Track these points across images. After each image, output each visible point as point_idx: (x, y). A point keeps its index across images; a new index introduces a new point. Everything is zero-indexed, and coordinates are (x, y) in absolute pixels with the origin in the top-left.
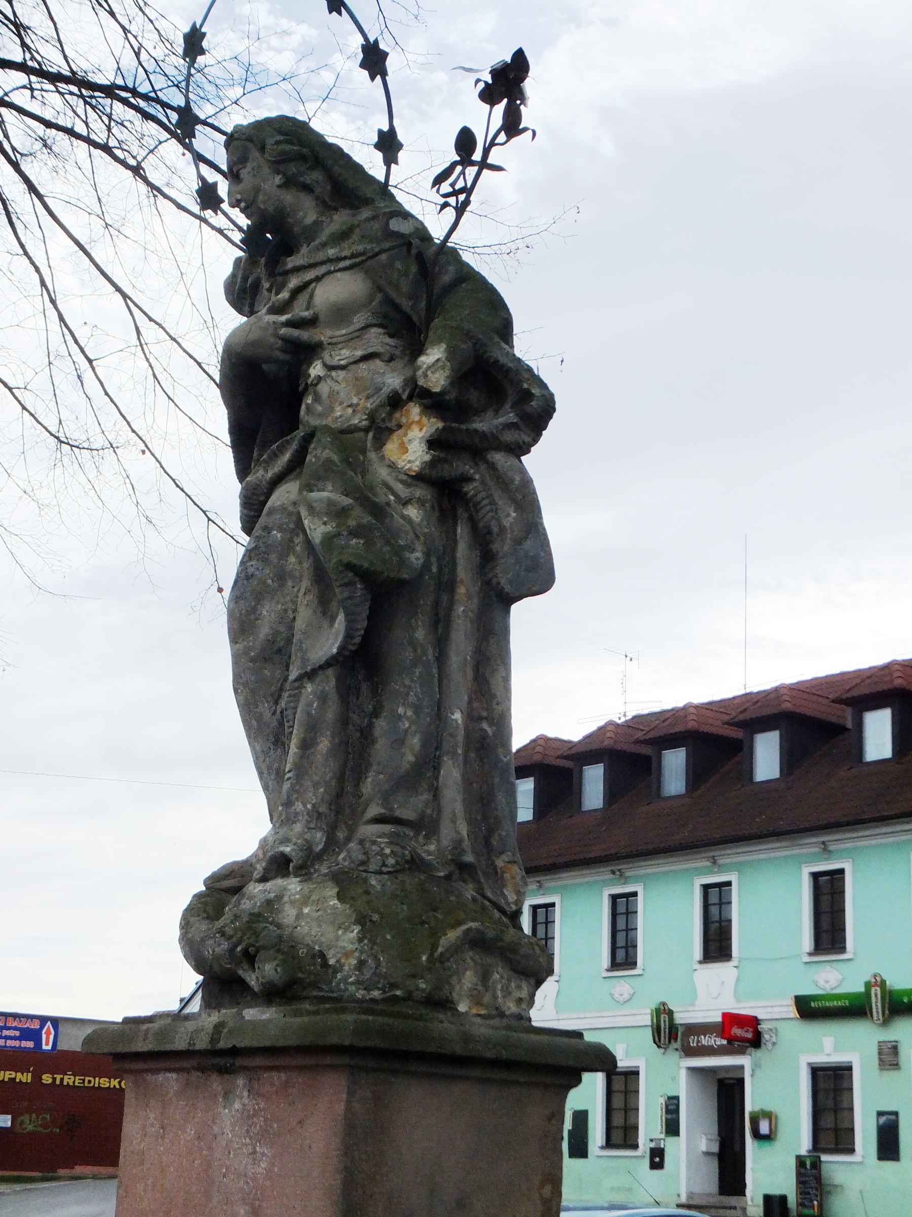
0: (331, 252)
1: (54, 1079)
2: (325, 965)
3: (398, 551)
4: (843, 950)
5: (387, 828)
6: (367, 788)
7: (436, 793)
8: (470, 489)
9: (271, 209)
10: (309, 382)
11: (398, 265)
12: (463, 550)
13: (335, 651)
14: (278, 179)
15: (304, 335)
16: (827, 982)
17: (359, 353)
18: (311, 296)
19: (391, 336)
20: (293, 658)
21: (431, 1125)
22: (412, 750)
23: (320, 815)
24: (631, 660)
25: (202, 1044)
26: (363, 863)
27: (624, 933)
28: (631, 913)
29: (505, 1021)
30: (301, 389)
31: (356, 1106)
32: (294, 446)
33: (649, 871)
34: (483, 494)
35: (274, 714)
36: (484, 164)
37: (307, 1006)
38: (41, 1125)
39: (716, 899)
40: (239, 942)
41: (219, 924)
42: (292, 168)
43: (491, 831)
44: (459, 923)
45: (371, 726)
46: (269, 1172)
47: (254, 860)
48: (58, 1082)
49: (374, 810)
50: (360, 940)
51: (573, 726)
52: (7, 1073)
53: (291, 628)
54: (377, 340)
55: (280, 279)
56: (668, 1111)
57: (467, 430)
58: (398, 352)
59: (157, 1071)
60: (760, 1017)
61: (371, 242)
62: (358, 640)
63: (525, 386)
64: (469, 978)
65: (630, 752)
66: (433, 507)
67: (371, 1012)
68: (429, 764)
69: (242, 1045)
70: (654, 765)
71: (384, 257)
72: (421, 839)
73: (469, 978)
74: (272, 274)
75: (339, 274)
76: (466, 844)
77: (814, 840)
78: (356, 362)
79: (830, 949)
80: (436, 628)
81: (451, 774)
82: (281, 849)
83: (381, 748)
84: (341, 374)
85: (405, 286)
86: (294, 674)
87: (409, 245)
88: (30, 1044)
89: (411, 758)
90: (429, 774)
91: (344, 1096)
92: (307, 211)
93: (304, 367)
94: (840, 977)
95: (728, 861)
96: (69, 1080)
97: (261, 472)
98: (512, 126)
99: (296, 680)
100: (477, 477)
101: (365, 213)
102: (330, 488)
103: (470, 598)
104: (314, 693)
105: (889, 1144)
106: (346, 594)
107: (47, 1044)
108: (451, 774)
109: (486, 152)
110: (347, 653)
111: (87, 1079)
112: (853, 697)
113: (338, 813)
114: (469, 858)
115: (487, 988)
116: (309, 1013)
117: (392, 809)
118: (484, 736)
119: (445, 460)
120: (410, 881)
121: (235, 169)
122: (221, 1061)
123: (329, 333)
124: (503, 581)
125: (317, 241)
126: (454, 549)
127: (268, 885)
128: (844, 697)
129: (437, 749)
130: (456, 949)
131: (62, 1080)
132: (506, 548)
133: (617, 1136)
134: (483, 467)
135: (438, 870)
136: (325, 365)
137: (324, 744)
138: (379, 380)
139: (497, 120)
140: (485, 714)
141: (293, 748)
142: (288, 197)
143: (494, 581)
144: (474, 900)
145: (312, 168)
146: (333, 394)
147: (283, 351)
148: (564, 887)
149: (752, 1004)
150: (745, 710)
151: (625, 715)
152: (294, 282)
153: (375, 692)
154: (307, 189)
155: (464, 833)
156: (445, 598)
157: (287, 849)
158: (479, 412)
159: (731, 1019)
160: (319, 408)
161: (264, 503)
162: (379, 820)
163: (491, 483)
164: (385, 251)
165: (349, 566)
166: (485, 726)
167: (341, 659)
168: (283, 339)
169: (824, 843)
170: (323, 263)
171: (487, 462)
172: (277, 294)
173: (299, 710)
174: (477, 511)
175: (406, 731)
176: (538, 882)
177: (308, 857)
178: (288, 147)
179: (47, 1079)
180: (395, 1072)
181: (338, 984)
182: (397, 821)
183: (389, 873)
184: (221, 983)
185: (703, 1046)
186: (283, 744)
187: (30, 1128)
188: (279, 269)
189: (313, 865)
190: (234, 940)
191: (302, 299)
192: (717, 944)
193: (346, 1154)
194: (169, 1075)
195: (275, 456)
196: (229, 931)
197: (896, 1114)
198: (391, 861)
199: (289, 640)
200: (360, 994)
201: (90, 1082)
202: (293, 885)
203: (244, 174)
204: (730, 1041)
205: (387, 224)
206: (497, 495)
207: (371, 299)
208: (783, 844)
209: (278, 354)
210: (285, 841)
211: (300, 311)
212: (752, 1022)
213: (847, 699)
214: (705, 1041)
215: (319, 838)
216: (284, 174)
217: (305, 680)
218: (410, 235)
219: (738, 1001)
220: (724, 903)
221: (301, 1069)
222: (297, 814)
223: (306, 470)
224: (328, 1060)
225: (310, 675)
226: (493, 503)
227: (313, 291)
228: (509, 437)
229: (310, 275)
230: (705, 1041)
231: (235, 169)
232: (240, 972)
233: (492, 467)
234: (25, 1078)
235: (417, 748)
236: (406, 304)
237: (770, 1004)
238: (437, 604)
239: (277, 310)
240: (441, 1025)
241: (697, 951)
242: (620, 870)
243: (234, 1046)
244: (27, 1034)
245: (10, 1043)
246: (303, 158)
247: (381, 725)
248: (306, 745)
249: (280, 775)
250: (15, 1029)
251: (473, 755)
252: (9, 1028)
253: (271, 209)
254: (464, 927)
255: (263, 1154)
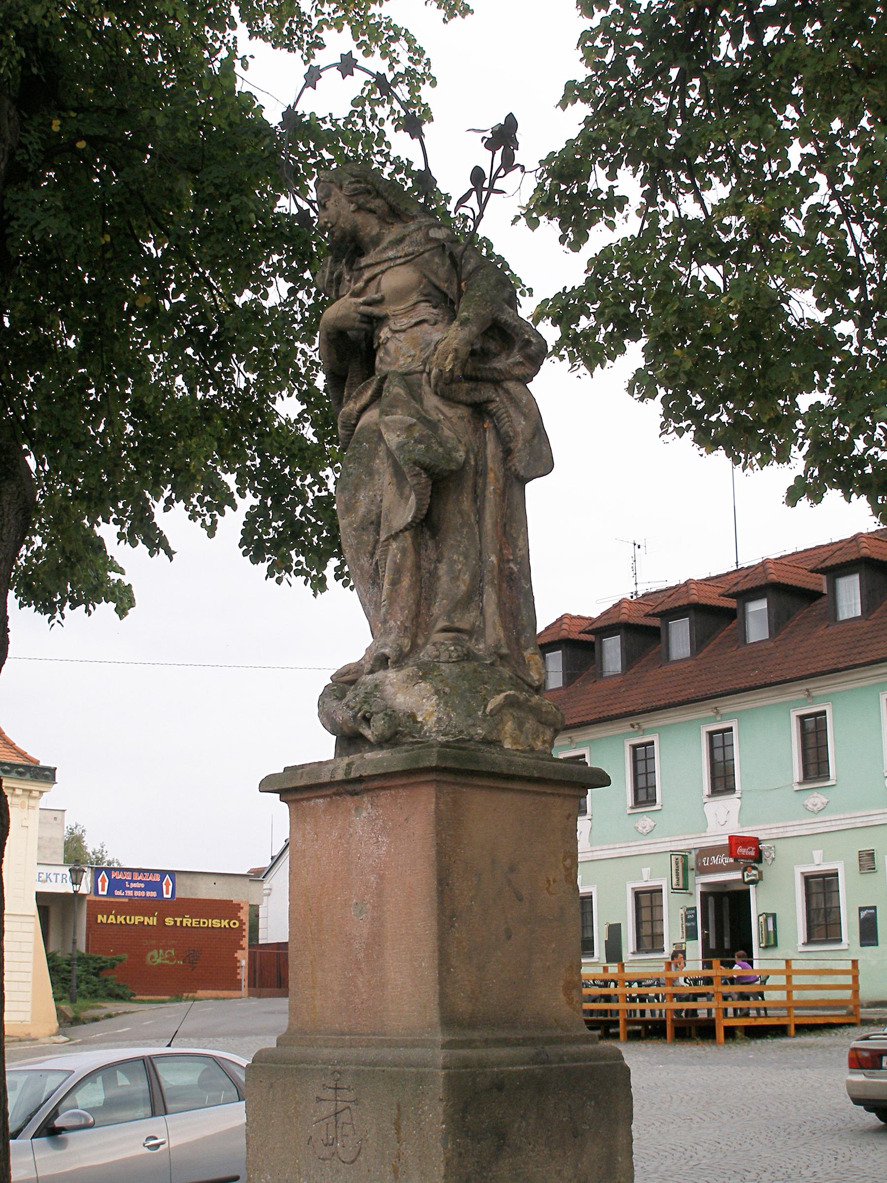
0: (391, 254)
1: (175, 922)
2: (416, 722)
3: (449, 452)
4: (827, 777)
5: (451, 635)
6: (436, 610)
7: (482, 612)
8: (491, 406)
9: (348, 227)
10: (381, 341)
11: (437, 260)
12: (492, 448)
13: (410, 519)
14: (352, 207)
15: (375, 310)
16: (815, 805)
17: (414, 321)
18: (379, 284)
19: (435, 307)
20: (382, 527)
21: (492, 815)
22: (464, 583)
23: (406, 628)
24: (639, 547)
25: (340, 776)
26: (438, 657)
27: (644, 776)
28: (649, 758)
29: (535, 755)
30: (375, 346)
31: (442, 807)
32: (374, 386)
33: (661, 723)
34: (502, 410)
35: (371, 565)
36: (491, 190)
37: (406, 747)
38: (167, 959)
39: (719, 743)
40: (360, 710)
41: (344, 701)
42: (361, 200)
43: (519, 634)
44: (502, 691)
45: (436, 568)
46: (388, 852)
47: (363, 662)
48: (178, 924)
49: (441, 624)
50: (438, 705)
51: (592, 607)
52: (137, 918)
53: (380, 507)
54: (425, 311)
55: (356, 273)
56: (687, 920)
57: (490, 369)
58: (440, 319)
59: (308, 799)
60: (760, 838)
61: (417, 245)
62: (424, 512)
63: (527, 337)
64: (509, 726)
65: (640, 626)
66: (469, 421)
67: (449, 747)
68: (475, 592)
69: (366, 774)
70: (663, 638)
71: (426, 255)
72: (473, 641)
73: (509, 726)
74: (351, 269)
75: (397, 268)
76: (503, 642)
77: (798, 688)
78: (411, 327)
79: (815, 778)
80: (476, 502)
81: (490, 599)
82: (383, 651)
83: (444, 582)
84: (402, 336)
85: (443, 272)
86: (383, 537)
87: (444, 246)
88: (154, 894)
89: (463, 588)
90: (477, 599)
91: (434, 800)
92: (371, 226)
93: (376, 332)
94: (825, 800)
95: (730, 710)
96: (187, 922)
97: (352, 405)
98: (508, 164)
99: (385, 541)
100: (498, 399)
101: (412, 226)
102: (400, 412)
103: (497, 480)
104: (397, 548)
105: (869, 932)
106: (415, 482)
107: (167, 893)
108: (490, 599)
109: (492, 183)
110: (418, 521)
111: (202, 921)
112: (827, 567)
113: (417, 627)
114: (504, 651)
115: (521, 731)
116: (407, 751)
117: (453, 622)
118: (512, 573)
119: (476, 390)
120: (469, 667)
121: (323, 202)
122: (350, 788)
123: (392, 308)
124: (518, 468)
125: (381, 247)
126: (485, 448)
127: (376, 675)
128: (819, 567)
129: (481, 581)
130: (500, 709)
131: (182, 922)
132: (520, 446)
133: (646, 941)
134: (501, 392)
135: (485, 660)
136: (390, 329)
137: (406, 582)
138: (428, 337)
139: (498, 162)
140: (511, 558)
141: (386, 586)
142: (359, 218)
143: (513, 468)
144: (511, 678)
145: (374, 198)
146: (398, 349)
147: (362, 322)
148: (591, 741)
149: (754, 828)
150: (737, 583)
151: (636, 594)
152: (367, 275)
153: (437, 547)
154: (372, 211)
155: (502, 635)
156: (480, 481)
157: (387, 651)
158: (496, 355)
159: (736, 841)
160: (389, 359)
161: (355, 425)
162: (445, 630)
163: (508, 404)
164: (428, 250)
165: (416, 463)
166: (512, 565)
167: (414, 525)
168: (363, 315)
169: (807, 690)
170: (385, 261)
171: (503, 388)
172: (355, 283)
173: (388, 561)
174: (499, 423)
175: (460, 571)
176: (570, 738)
177: (400, 655)
178: (358, 186)
179: (169, 921)
180: (465, 785)
181: (425, 733)
182: (458, 630)
183: (454, 662)
184: (349, 741)
185: (714, 865)
186: (378, 584)
187: (159, 961)
188: (355, 267)
189: (403, 660)
190: (356, 709)
191: (373, 285)
192: (722, 781)
193: (437, 836)
194: (317, 800)
195: (361, 393)
196: (352, 704)
197: (875, 908)
198: (454, 655)
199: (379, 516)
200: (441, 738)
201: (204, 923)
202: (392, 675)
203: (328, 204)
204: (736, 860)
205: (427, 233)
206: (512, 411)
207: (420, 283)
208: (774, 693)
209: (357, 324)
210: (385, 645)
211: (371, 294)
212: (755, 842)
213: (822, 568)
214: (715, 860)
215: (407, 642)
216: (357, 203)
217: (391, 540)
218: (444, 239)
219: (742, 826)
220: (727, 746)
221: (404, 786)
222: (391, 628)
223: (385, 401)
224: (423, 778)
225: (395, 537)
226: (509, 416)
227: (380, 280)
228: (517, 371)
229: (377, 269)
230: (715, 860)
231: (323, 202)
232: (361, 730)
233: (507, 391)
234: (153, 921)
235: (468, 581)
236: (444, 286)
237: (768, 826)
238: (475, 485)
239: (356, 294)
240: (494, 754)
241: (707, 788)
242: (638, 724)
243: (361, 776)
244: (150, 886)
245: (137, 893)
246: (369, 192)
247: (443, 568)
248: (394, 583)
249: (377, 606)
250: (141, 881)
251: (505, 585)
252: (136, 882)
253: (348, 227)
254: (505, 694)
255: (383, 842)
